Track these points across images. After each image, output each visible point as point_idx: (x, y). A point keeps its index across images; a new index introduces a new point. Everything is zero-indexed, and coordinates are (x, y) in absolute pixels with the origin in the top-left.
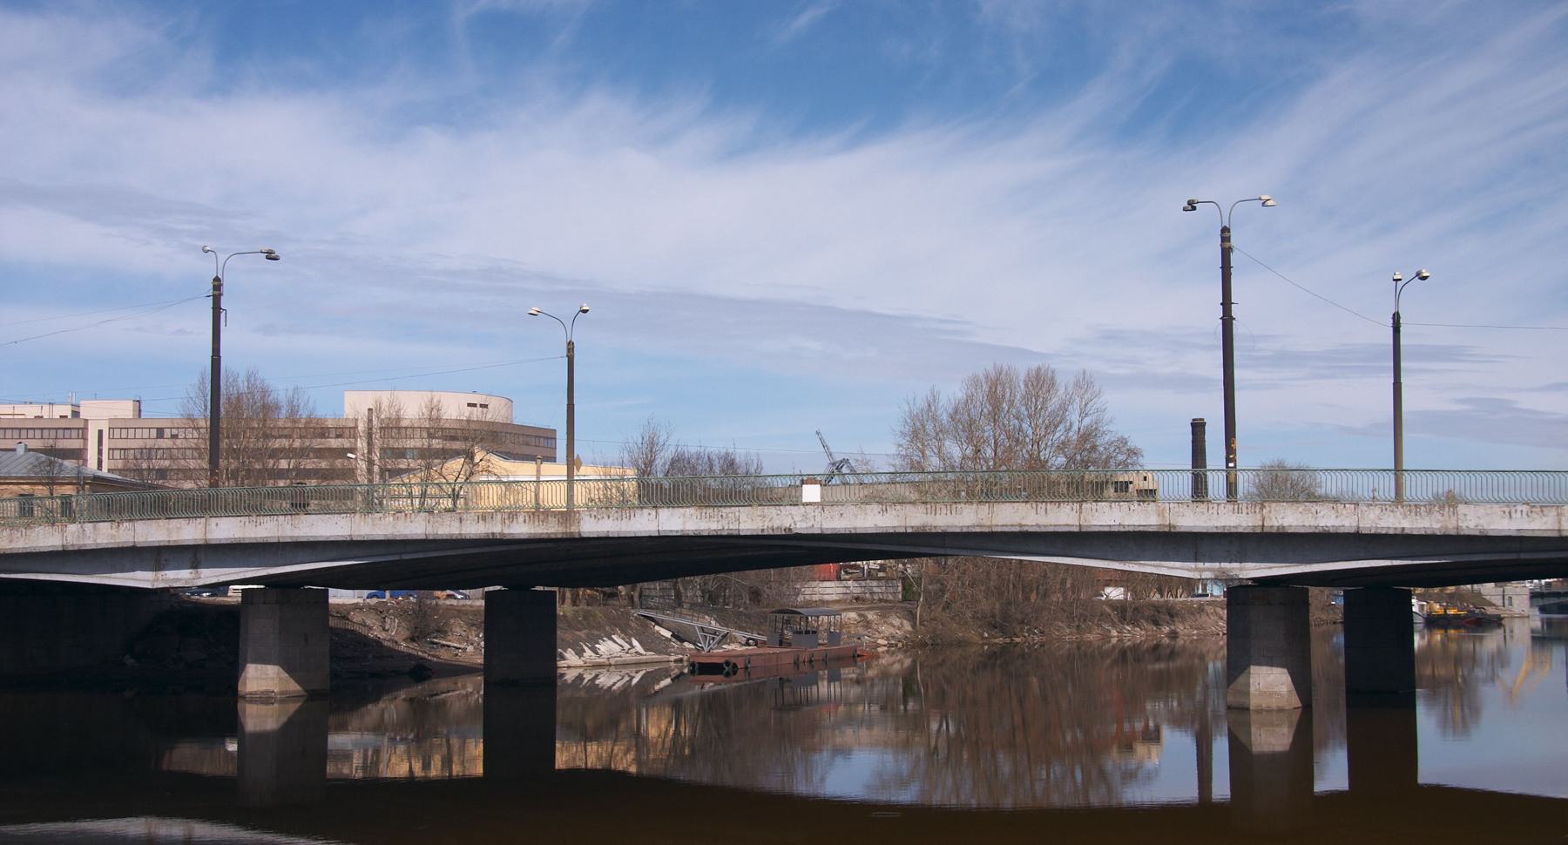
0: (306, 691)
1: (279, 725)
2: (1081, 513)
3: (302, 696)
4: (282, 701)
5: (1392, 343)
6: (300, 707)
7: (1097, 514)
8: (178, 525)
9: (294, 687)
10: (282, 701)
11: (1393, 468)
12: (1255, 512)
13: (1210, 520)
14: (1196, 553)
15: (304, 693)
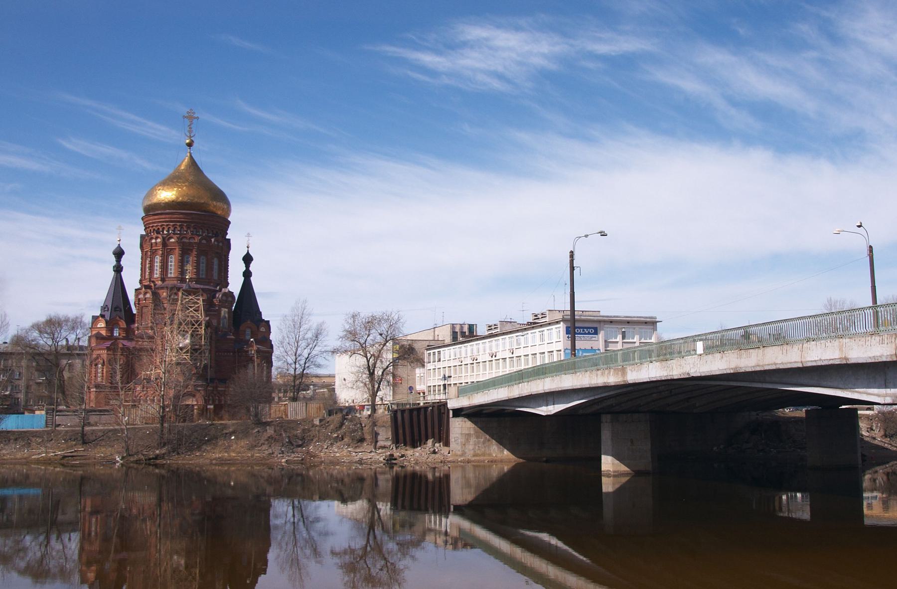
0: (633, 471)
1: (614, 489)
2: (802, 352)
3: (630, 474)
4: (614, 476)
5: (16, 415)
6: (629, 479)
7: (809, 352)
8: (79, 439)
9: (623, 468)
10: (614, 476)
11: (871, 305)
12: (892, 342)
13: (866, 351)
14: (885, 381)
15: (631, 472)
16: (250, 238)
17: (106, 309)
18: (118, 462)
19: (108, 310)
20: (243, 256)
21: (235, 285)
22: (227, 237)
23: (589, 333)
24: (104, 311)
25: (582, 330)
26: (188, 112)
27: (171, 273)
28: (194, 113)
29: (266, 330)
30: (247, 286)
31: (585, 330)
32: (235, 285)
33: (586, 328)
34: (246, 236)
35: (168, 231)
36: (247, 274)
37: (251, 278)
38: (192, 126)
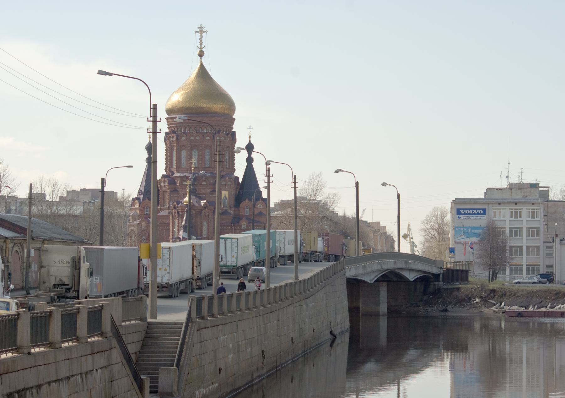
16: (251, 130)
17: (141, 193)
18: (264, 342)
19: (142, 194)
20: (245, 146)
21: (240, 172)
22: (233, 130)
23: (478, 214)
24: (140, 195)
25: (471, 211)
26: (199, 28)
27: (184, 165)
28: (204, 28)
29: (263, 206)
30: (250, 171)
31: (475, 211)
32: (240, 172)
33: (475, 209)
34: (248, 128)
35: (181, 131)
36: (250, 160)
37: (253, 164)
38: (202, 39)
